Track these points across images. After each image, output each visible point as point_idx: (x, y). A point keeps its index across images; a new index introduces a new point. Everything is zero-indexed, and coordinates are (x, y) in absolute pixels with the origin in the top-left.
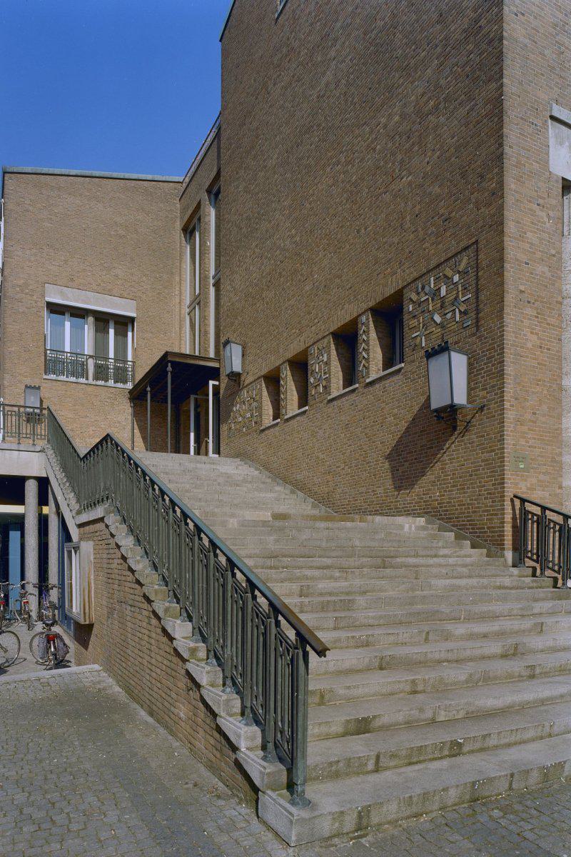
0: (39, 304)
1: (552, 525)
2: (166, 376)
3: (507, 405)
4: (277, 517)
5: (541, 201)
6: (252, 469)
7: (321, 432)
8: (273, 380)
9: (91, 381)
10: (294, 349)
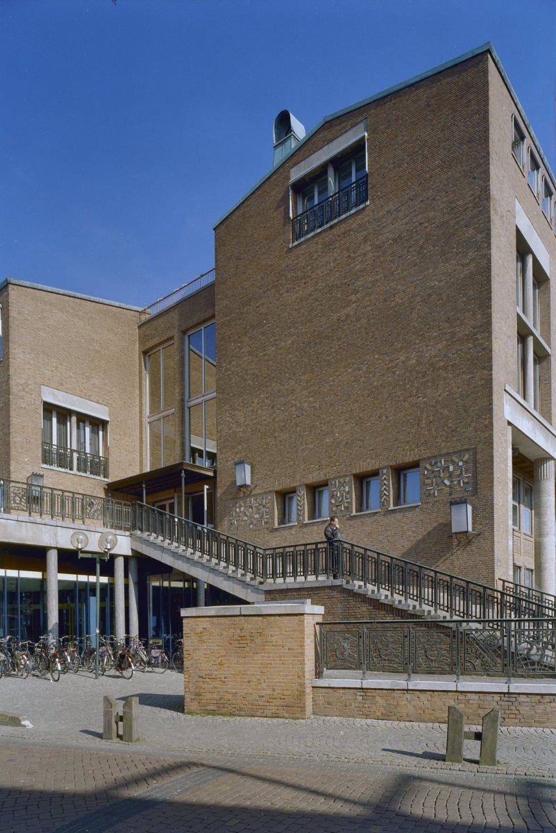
1: (383, 563)
2: (181, 480)
8: (285, 496)
9: (75, 471)
10: (314, 477)
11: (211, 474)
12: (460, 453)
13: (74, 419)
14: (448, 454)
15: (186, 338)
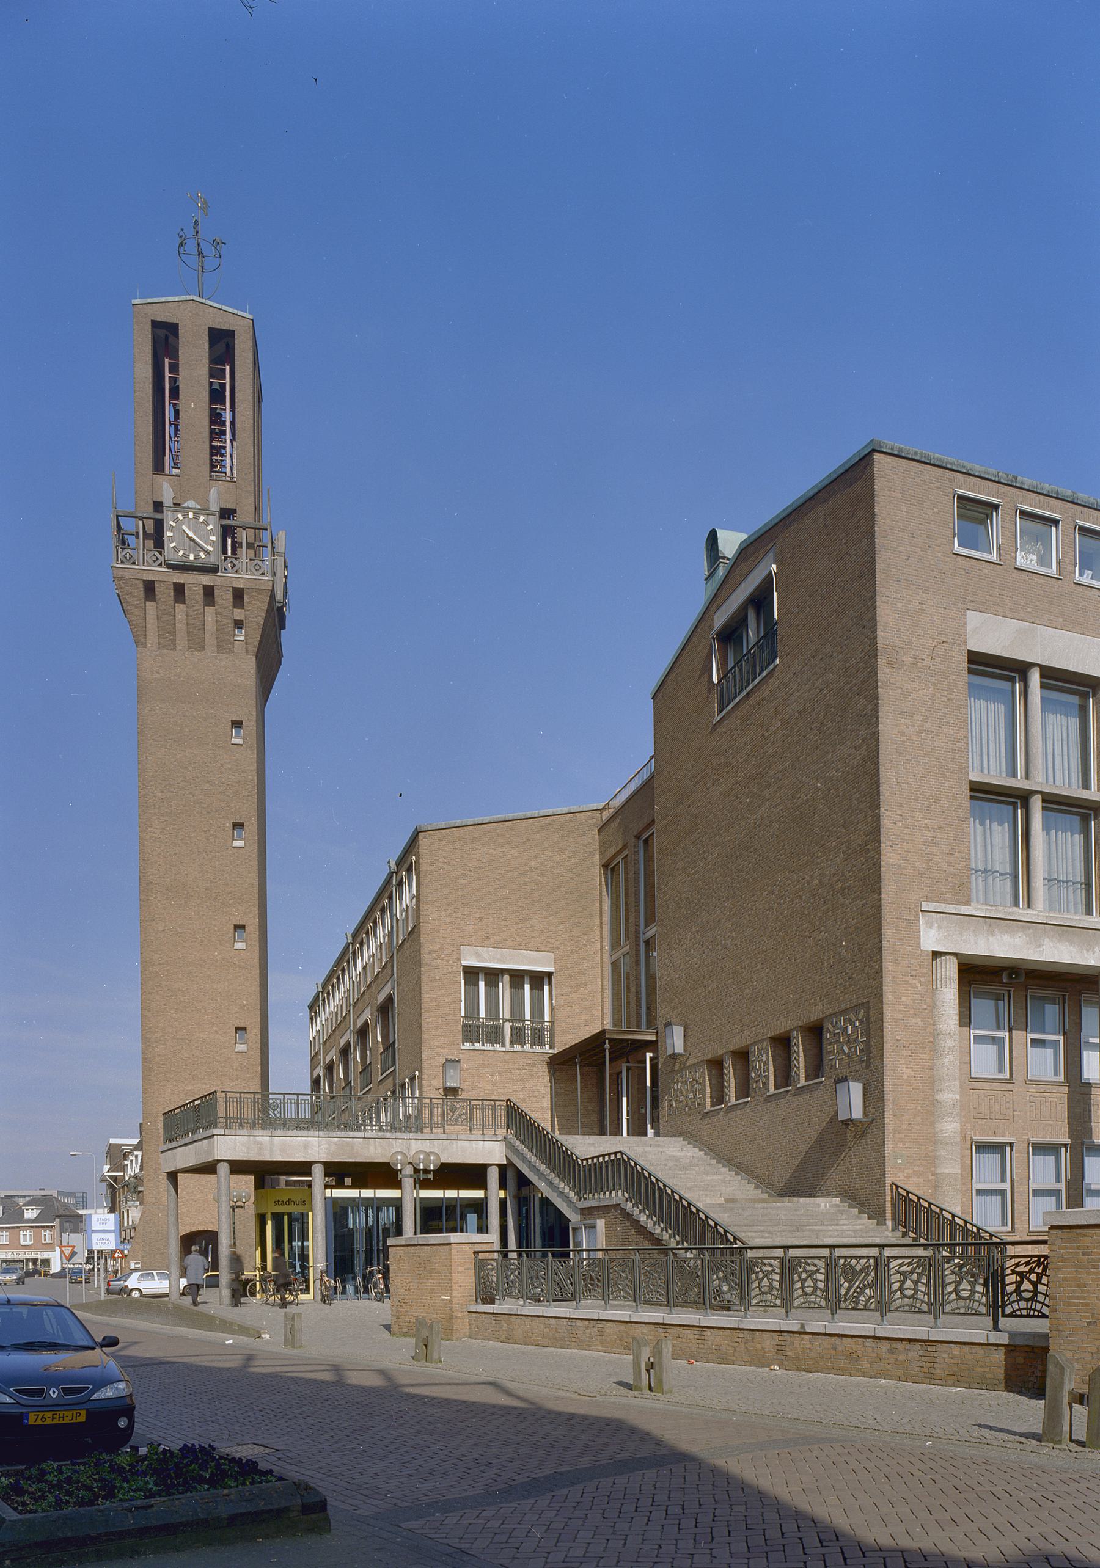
0: (455, 969)
3: (887, 1120)
4: (727, 1200)
5: (913, 973)
6: (697, 1150)
7: (762, 1123)
8: (716, 1064)
9: (508, 1047)
10: (737, 1043)
11: (653, 1038)
12: (855, 1008)
13: (507, 978)
14: (845, 1010)
15: (641, 844)
